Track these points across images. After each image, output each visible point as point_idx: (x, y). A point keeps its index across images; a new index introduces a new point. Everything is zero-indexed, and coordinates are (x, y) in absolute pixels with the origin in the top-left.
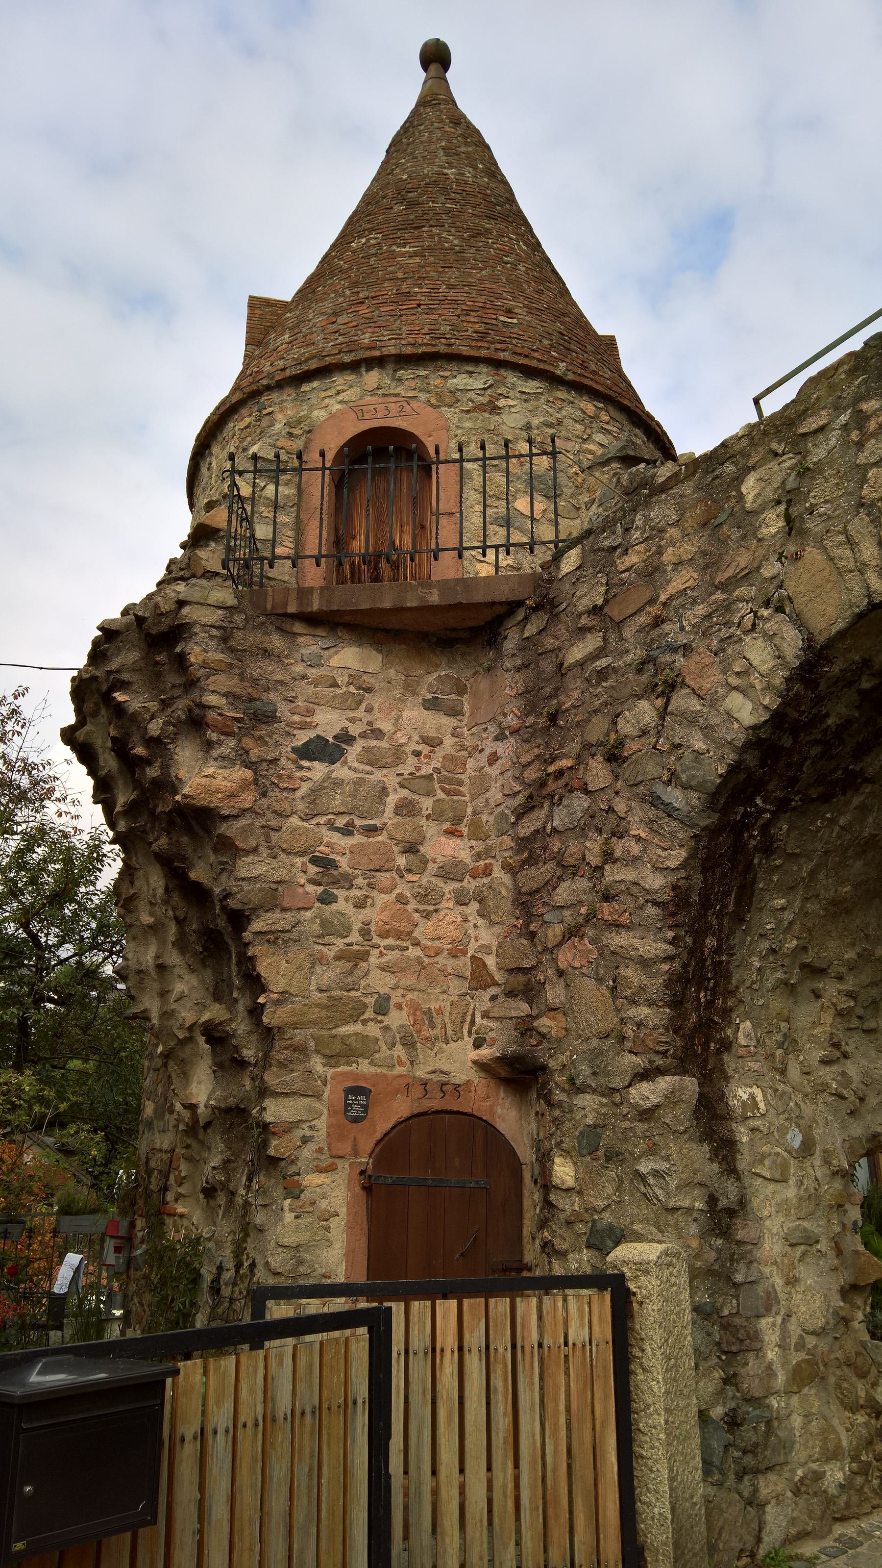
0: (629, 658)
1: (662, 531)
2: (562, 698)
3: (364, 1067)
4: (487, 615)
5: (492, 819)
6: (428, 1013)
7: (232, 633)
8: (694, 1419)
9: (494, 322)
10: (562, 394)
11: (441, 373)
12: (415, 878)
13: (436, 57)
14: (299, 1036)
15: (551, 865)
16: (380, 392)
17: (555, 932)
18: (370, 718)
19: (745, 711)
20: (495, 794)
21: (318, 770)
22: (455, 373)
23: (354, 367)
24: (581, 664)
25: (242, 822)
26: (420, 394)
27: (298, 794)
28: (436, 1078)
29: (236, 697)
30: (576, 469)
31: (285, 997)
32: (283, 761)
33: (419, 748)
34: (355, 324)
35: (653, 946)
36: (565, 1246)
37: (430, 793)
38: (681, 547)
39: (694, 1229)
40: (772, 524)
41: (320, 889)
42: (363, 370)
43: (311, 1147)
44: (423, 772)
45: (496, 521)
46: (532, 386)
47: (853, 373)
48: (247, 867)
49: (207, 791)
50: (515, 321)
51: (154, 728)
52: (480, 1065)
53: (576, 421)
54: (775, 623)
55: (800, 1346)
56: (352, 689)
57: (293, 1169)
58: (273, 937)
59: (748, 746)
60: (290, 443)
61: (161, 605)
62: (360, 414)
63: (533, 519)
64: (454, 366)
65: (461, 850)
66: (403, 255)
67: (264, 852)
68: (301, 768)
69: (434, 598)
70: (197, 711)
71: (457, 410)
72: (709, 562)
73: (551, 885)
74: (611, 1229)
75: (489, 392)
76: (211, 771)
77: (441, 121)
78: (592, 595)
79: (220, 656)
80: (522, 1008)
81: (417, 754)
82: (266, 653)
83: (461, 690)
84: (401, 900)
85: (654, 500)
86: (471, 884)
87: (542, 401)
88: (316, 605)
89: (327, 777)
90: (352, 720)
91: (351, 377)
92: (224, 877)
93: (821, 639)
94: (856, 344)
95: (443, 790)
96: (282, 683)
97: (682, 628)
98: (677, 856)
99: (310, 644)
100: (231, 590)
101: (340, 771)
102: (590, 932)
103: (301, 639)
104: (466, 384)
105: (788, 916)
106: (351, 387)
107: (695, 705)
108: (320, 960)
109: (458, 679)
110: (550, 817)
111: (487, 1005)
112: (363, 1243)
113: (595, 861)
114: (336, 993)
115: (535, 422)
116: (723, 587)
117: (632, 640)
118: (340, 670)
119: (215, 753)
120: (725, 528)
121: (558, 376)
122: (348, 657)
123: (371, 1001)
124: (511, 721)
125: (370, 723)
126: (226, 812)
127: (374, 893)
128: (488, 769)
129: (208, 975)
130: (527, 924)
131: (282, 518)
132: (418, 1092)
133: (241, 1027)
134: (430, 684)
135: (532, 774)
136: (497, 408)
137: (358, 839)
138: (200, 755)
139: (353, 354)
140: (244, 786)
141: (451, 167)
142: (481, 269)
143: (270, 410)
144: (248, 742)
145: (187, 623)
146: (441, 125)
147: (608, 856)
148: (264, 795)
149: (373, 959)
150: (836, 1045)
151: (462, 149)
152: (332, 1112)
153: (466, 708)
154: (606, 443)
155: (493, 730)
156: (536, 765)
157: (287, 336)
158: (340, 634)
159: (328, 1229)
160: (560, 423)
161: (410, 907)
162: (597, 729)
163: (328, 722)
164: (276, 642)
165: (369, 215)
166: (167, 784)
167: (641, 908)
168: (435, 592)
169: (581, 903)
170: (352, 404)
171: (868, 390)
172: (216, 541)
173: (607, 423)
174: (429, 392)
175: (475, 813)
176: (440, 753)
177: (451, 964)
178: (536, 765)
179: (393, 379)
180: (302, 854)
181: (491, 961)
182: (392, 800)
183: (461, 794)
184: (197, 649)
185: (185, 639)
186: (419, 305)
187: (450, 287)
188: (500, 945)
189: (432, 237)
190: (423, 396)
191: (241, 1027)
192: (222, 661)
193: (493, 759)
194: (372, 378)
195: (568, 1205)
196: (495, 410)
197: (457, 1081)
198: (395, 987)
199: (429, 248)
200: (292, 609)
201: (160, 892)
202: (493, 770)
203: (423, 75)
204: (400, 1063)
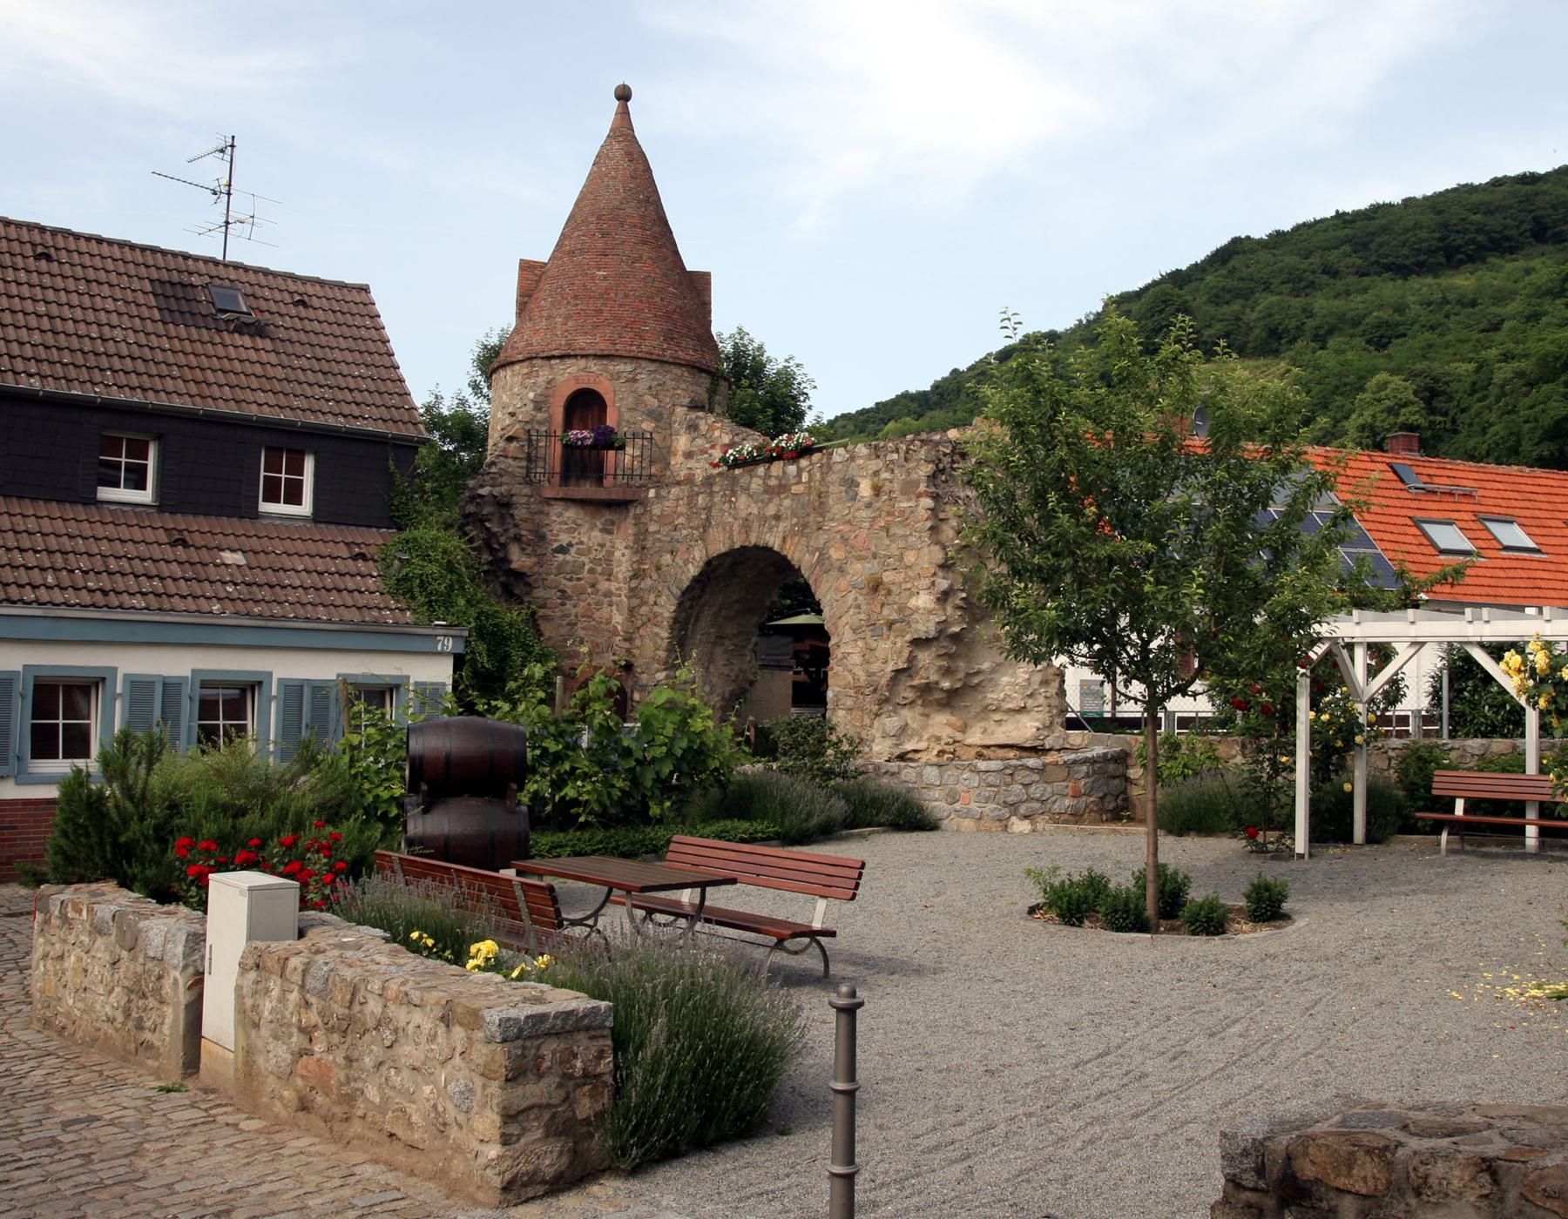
13: (624, 95)
17: (639, 623)
20: (623, 568)
21: (561, 557)
31: (550, 638)
35: (665, 634)
46: (652, 367)
51: (502, 540)
73: (640, 606)
80: (627, 645)
98: (673, 608)
101: (568, 558)
108: (560, 626)
122: (571, 513)
163: (564, 539)
166: (507, 560)
194: (582, 362)
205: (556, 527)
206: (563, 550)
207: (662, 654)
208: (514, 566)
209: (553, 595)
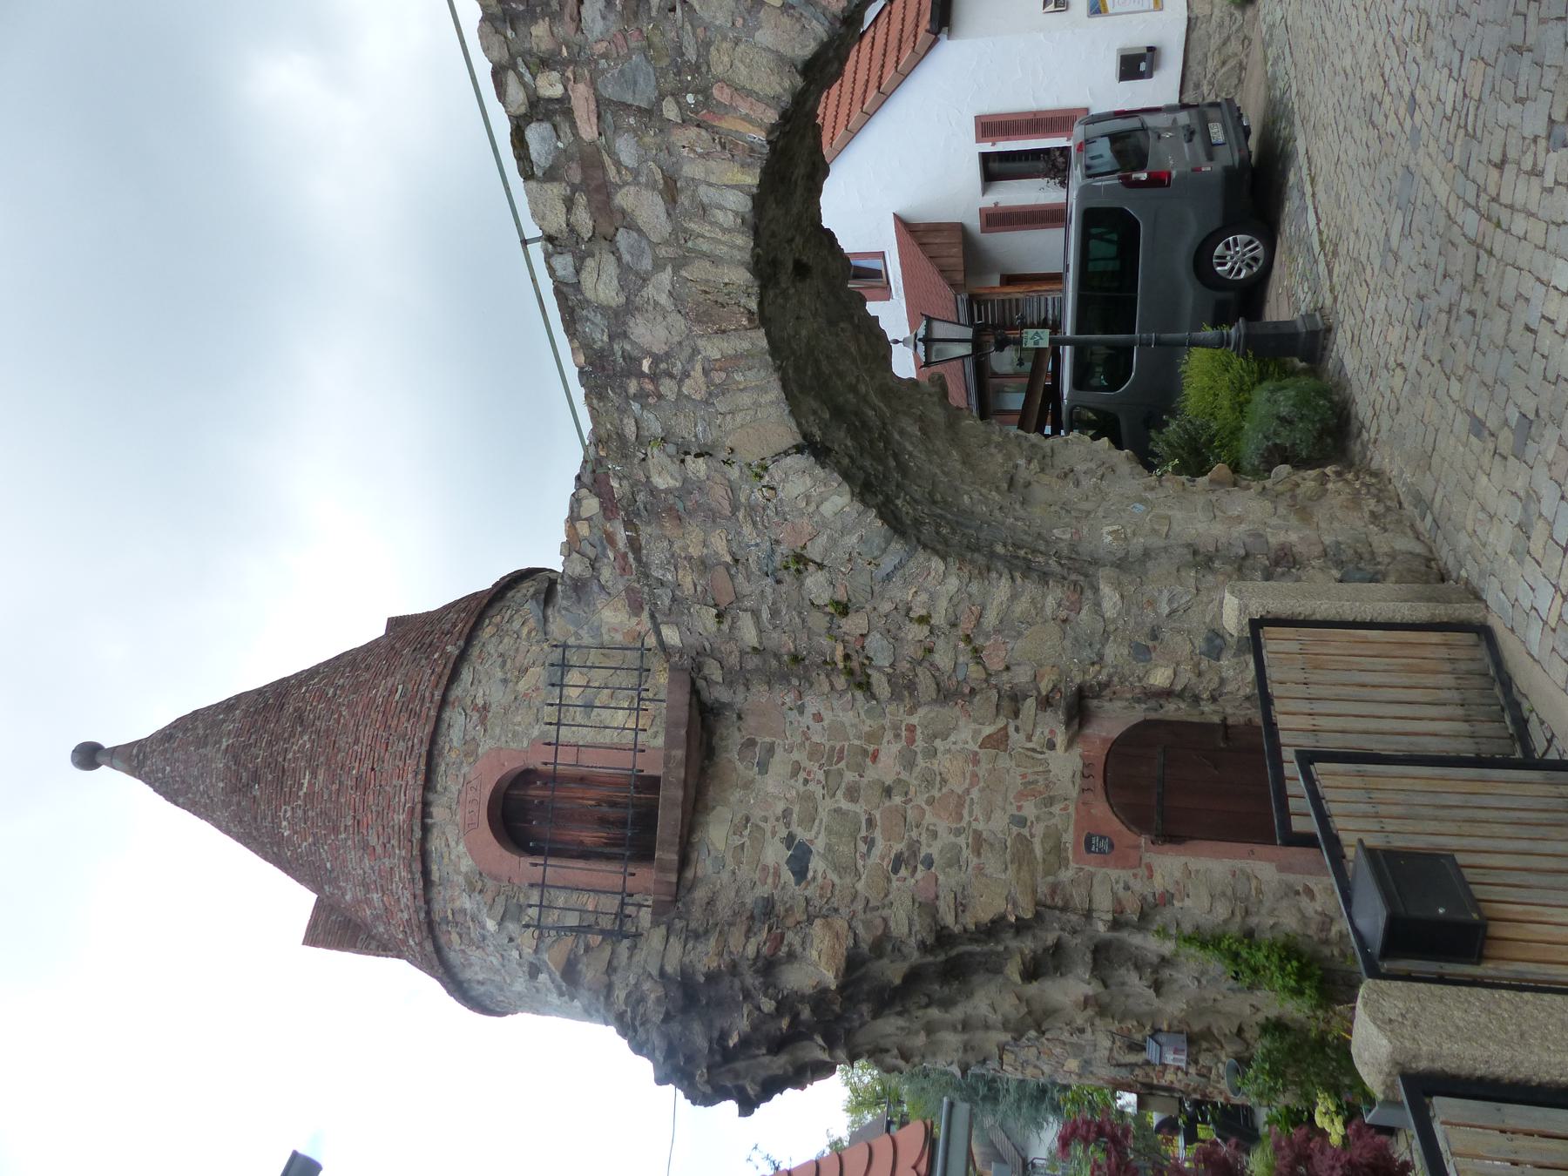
0: (768, 590)
2: (784, 651)
3: (1069, 838)
4: (696, 713)
5: (868, 722)
6: (1025, 784)
8: (1344, 585)
10: (475, 651)
12: (912, 789)
13: (89, 756)
14: (1043, 889)
15: (919, 670)
17: (975, 672)
18: (772, 819)
19: (838, 501)
20: (848, 717)
21: (816, 865)
23: (426, 829)
24: (760, 631)
25: (861, 930)
27: (837, 881)
28: (1078, 780)
29: (749, 930)
32: (807, 893)
33: (801, 781)
36: (1217, 679)
37: (840, 773)
38: (693, 541)
39: (1210, 577)
40: (697, 467)
41: (920, 867)
42: (429, 821)
43: (1132, 882)
44: (822, 778)
46: (466, 675)
47: (602, 397)
48: (899, 928)
49: (834, 957)
51: (768, 1005)
52: (1070, 744)
54: (776, 473)
55: (1284, 518)
56: (746, 833)
57: (1150, 899)
58: (961, 907)
59: (863, 501)
65: (890, 750)
67: (886, 912)
68: (814, 878)
70: (759, 964)
72: (713, 516)
74: (1209, 640)
76: (815, 953)
77: (165, 750)
79: (712, 941)
80: (1030, 705)
81: (806, 782)
83: (751, 743)
84: (931, 801)
86: (920, 744)
89: (824, 857)
90: (774, 834)
91: (435, 832)
92: (905, 950)
93: (799, 439)
94: (578, 393)
95: (838, 762)
96: (737, 892)
97: (757, 545)
98: (937, 564)
99: (703, 866)
101: (819, 845)
102: (979, 641)
103: (699, 873)
105: (975, 496)
107: (822, 540)
110: (880, 669)
111: (1021, 736)
112: (1207, 845)
113: (926, 630)
114: (1008, 857)
115: (500, 675)
116: (735, 508)
119: (799, 949)
122: (717, 834)
123: (1015, 830)
124: (789, 699)
125: (777, 820)
126: (851, 942)
127: (925, 823)
128: (825, 723)
129: (977, 979)
130: (963, 695)
131: (560, 902)
132: (1089, 796)
133: (1028, 945)
135: (841, 682)
137: (877, 833)
138: (796, 965)
140: (829, 926)
141: (220, 742)
143: (449, 913)
144: (790, 922)
147: (923, 620)
148: (836, 910)
149: (980, 826)
150: (1066, 475)
151: (201, 732)
152: (1105, 864)
153: (768, 739)
155: (794, 715)
156: (834, 678)
159: (1197, 871)
160: (501, 655)
161: (937, 795)
162: (818, 621)
163: (775, 854)
164: (700, 894)
166: (820, 998)
167: (970, 596)
168: (673, 753)
169: (956, 646)
171: (620, 387)
175: (859, 738)
176: (806, 763)
177: (985, 766)
178: (834, 678)
179: (443, 794)
180: (889, 880)
181: (988, 730)
182: (845, 805)
183: (842, 750)
184: (705, 960)
187: (356, 741)
188: (975, 721)
190: (466, 769)
191: (1028, 945)
193: (818, 718)
194: (439, 813)
195: (1186, 676)
196: (485, 708)
197: (1080, 765)
198: (1004, 809)
200: (673, 878)
201: (901, 1022)
202: (831, 714)
203: (104, 768)
204: (1065, 809)
205: (745, 872)
206: (799, 861)
207: (1052, 598)
208: (830, 979)
209: (906, 884)
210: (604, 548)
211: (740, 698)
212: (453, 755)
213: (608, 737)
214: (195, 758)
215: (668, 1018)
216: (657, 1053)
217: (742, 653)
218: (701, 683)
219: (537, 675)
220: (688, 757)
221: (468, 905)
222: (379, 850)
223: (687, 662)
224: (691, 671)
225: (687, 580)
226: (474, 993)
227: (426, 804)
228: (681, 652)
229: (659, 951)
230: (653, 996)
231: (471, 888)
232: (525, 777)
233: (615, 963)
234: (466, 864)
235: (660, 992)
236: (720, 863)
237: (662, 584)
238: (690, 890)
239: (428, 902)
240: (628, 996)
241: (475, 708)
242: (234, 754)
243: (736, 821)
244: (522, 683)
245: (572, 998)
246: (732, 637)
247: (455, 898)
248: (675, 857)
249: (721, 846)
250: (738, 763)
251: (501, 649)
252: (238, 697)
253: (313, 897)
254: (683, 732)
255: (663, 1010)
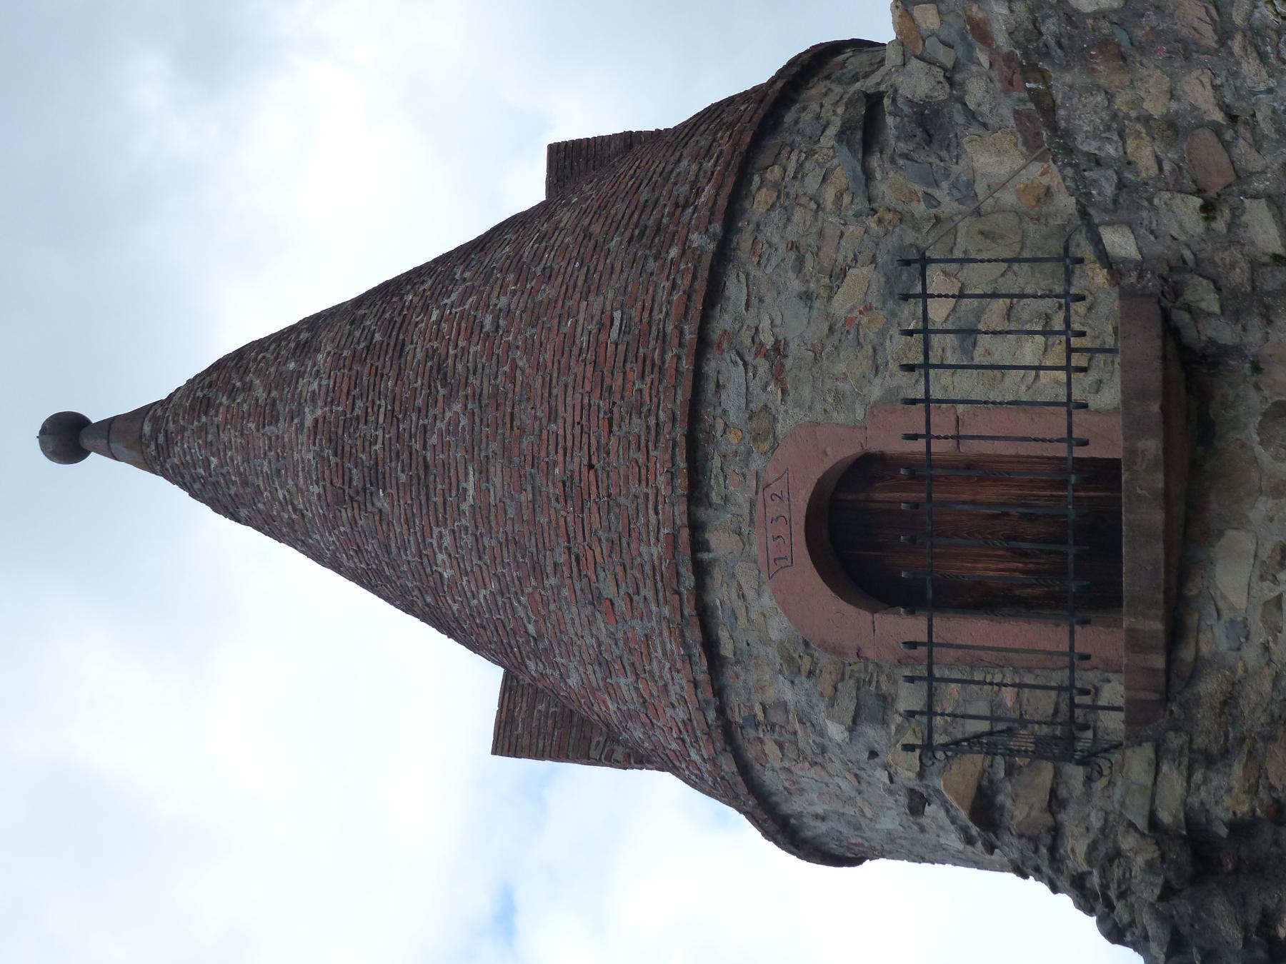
1: (1115, 116)
7: (1199, 751)
9: (622, 348)
10: (744, 242)
11: (718, 434)
13: (68, 437)
16: (745, 530)
22: (719, 411)
23: (701, 571)
26: (753, 467)
30: (872, 223)
34: (619, 570)
42: (706, 556)
45: (968, 352)
46: (735, 290)
50: (617, 315)
53: (789, 220)
60: (826, 675)
61: (1149, 856)
62: (782, 563)
63: (961, 295)
64: (708, 414)
66: (481, 491)
69: (1151, 446)
71: (782, 409)
72: (1184, 51)
75: (749, 358)
78: (1183, 215)
79: (1237, 769)
82: (1229, 701)
85: (1063, 124)
87: (759, 274)
88: (1156, 626)
91: (717, 575)
97: (1270, 91)
99: (1212, 639)
100: (1129, 752)
103: (1205, 650)
104: (738, 395)
106: (733, 576)
109: (1265, 415)
115: (796, 285)
116: (1225, 34)
117: (1269, 158)
118: (1253, 593)
120: (1139, 33)
121: (718, 247)
134: (1275, 458)
136: (776, 348)
139: (683, 571)
141: (300, 413)
142: (514, 366)
143: (758, 710)
145: (1186, 815)
146: (212, 430)
154: (820, 172)
157: (622, 681)
158: (1194, 592)
160: (793, 246)
164: (1210, 687)
165: (387, 547)
170: (764, 576)
172: (995, 793)
173: (785, 170)
174: (749, 453)
184: (1228, 801)
185: (1209, 822)
186: (591, 466)
187: (552, 415)
189: (445, 447)
190: (757, 463)
192: (1246, 766)
194: (720, 542)
196: (779, 349)
199: (470, 450)
200: (1159, 662)
210: (970, 48)
211: (1254, 336)
212: (733, 438)
213: (1013, 386)
214: (261, 443)
215: (1168, 892)
216: (1153, 946)
217: (1255, 265)
218: (1181, 317)
219: (862, 282)
220: (1167, 450)
221: (789, 696)
222: (621, 606)
223: (1151, 283)
224: (1160, 297)
225: (1144, 154)
226: (808, 834)
227: (696, 528)
228: (1140, 268)
229: (1140, 786)
230: (1140, 860)
231: (792, 667)
232: (866, 469)
233: (1062, 792)
234: (778, 627)
235: (1151, 852)
236: (1241, 631)
237: (1098, 162)
238: (1193, 676)
239: (719, 691)
240: (1093, 847)
241: (760, 350)
242: (332, 436)
243: (1264, 554)
244: (838, 299)
245: (991, 848)
246: (1233, 237)
247: (763, 684)
248: (1158, 626)
249: (1239, 601)
250: (1259, 449)
251: (792, 233)
252: (314, 323)
253: (93, 454)
254: (1155, 408)
255: (1160, 881)
